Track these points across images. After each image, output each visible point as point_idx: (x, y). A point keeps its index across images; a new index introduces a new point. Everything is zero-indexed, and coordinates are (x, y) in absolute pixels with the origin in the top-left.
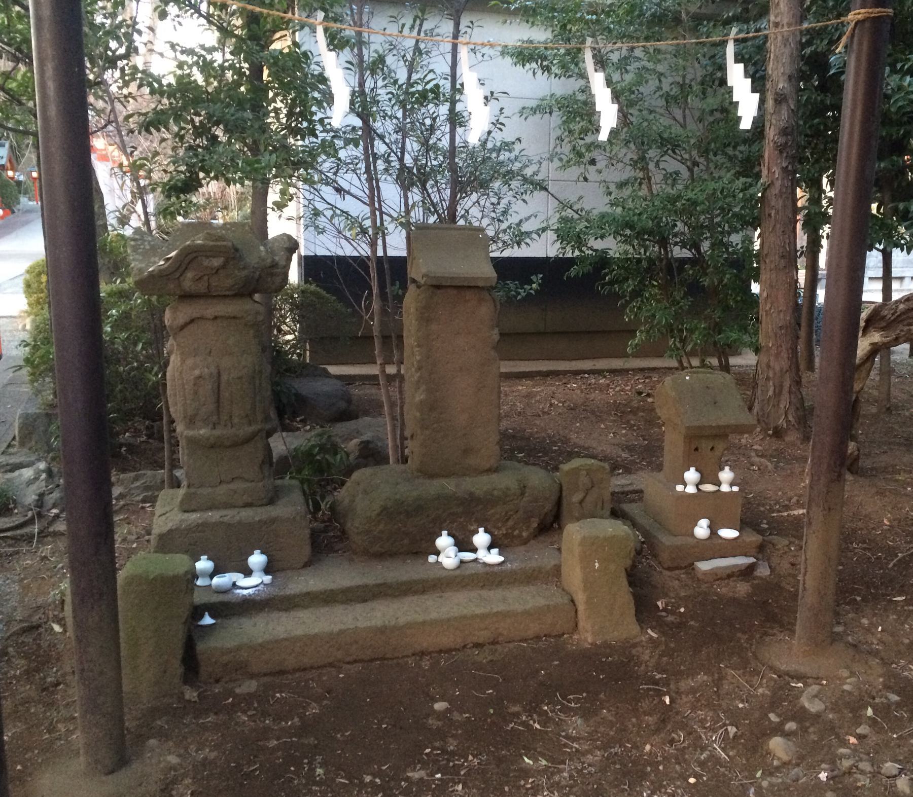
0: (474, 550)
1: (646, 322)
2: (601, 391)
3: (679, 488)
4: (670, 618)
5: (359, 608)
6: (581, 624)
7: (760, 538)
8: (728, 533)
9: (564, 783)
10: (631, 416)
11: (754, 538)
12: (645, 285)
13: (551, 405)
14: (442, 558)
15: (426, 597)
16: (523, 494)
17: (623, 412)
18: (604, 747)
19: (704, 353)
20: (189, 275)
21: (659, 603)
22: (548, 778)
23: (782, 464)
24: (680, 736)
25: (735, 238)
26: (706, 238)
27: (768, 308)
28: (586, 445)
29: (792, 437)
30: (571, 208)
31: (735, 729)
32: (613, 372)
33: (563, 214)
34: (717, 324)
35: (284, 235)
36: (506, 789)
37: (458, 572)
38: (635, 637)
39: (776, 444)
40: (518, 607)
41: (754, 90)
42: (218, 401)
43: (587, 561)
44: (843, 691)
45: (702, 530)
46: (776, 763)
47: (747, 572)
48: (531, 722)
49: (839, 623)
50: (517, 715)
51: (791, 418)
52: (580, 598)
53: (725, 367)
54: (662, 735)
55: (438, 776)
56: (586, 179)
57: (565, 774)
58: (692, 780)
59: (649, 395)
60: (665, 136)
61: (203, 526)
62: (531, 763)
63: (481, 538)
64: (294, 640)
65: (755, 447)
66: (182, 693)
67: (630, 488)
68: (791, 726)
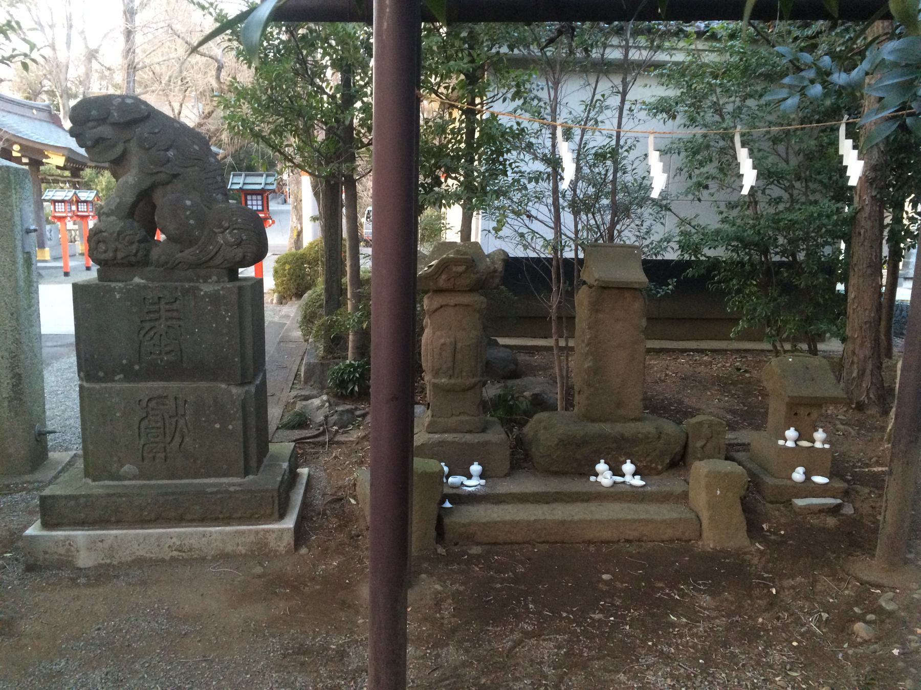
0: (623, 475)
1: (747, 314)
2: (706, 366)
3: (781, 442)
4: (773, 537)
5: (546, 507)
6: (705, 535)
7: (845, 485)
8: (819, 480)
9: (700, 634)
10: (732, 387)
11: (840, 485)
12: (747, 284)
13: (666, 375)
14: (600, 479)
15: (591, 504)
16: (659, 437)
17: (725, 384)
18: (728, 616)
19: (794, 340)
20: (444, 277)
21: (764, 526)
22: (689, 630)
23: (863, 432)
24: (784, 616)
25: (828, 250)
26: (803, 250)
27: (855, 307)
28: (697, 407)
29: (873, 411)
30: (690, 224)
31: (827, 615)
32: (714, 351)
33: (683, 228)
34: (808, 317)
35: (501, 250)
36: (660, 632)
37: (611, 490)
38: (746, 547)
39: (858, 416)
40: (658, 518)
41: (859, 159)
42: (454, 361)
43: (709, 487)
44: (913, 598)
45: (798, 475)
46: (858, 640)
47: (835, 510)
48: (673, 594)
49: (911, 552)
50: (662, 589)
51: (871, 396)
52: (705, 516)
53: (814, 352)
54: (771, 613)
55: (612, 619)
56: (699, 200)
57: (701, 629)
58: (795, 644)
59: (746, 371)
60: (772, 170)
61: (441, 443)
62: (676, 619)
63: (628, 467)
64: (505, 523)
65: (839, 417)
66: (436, 549)
67: (735, 441)
68: (871, 617)
